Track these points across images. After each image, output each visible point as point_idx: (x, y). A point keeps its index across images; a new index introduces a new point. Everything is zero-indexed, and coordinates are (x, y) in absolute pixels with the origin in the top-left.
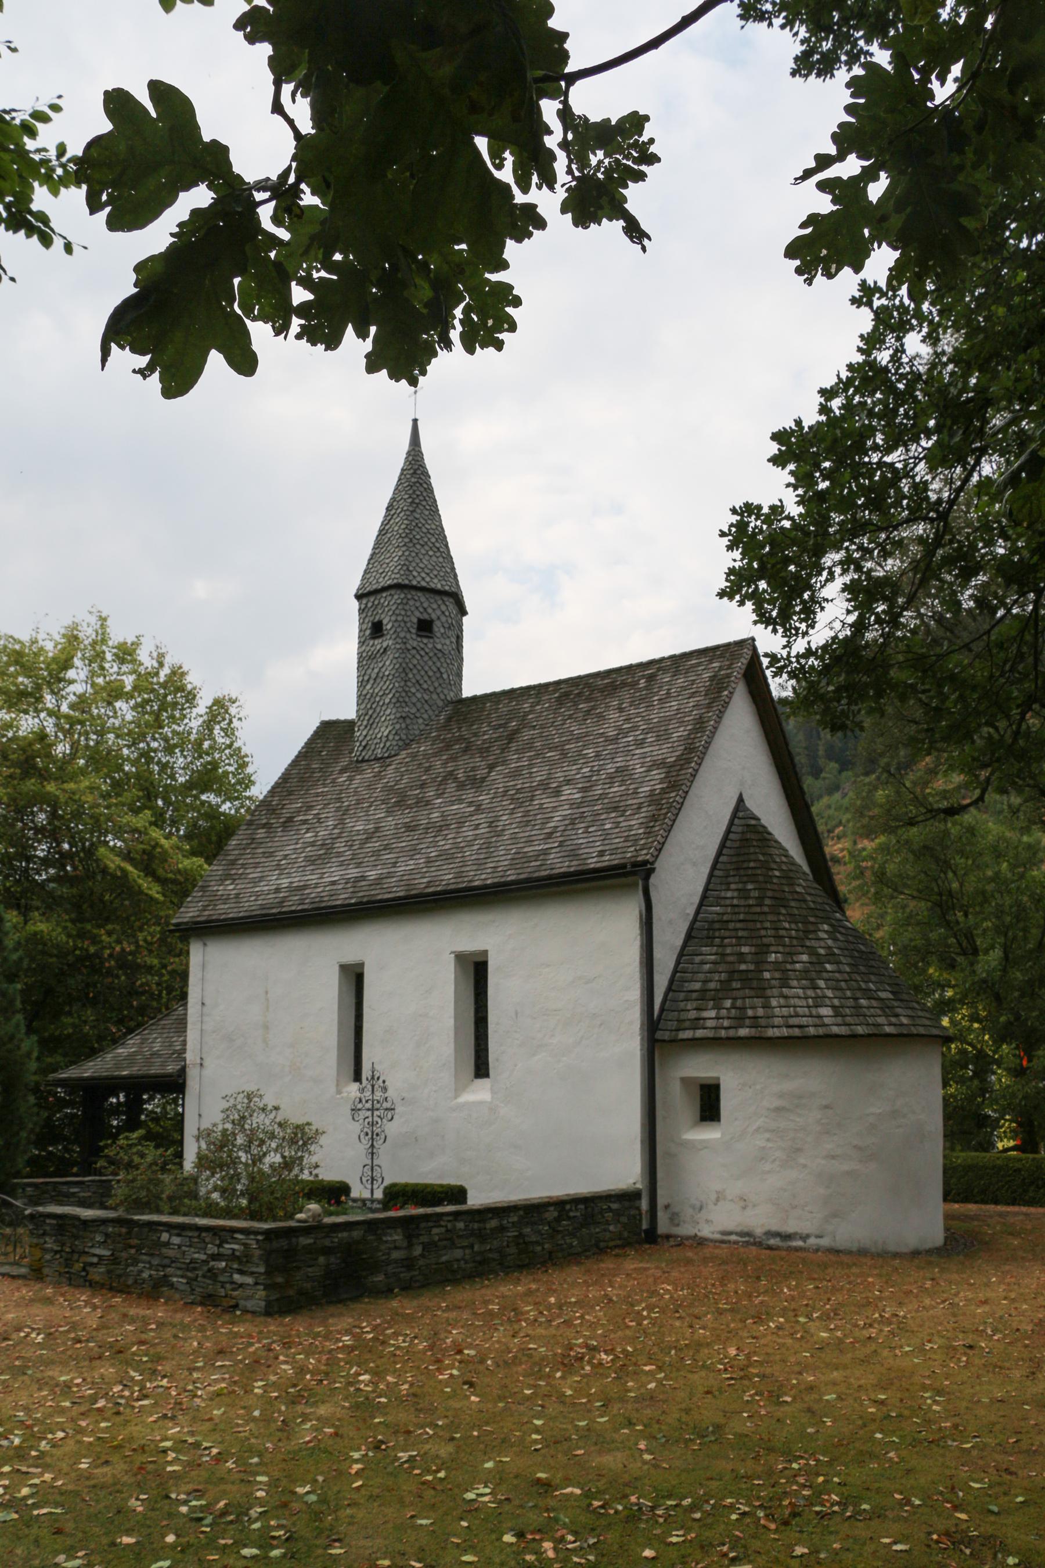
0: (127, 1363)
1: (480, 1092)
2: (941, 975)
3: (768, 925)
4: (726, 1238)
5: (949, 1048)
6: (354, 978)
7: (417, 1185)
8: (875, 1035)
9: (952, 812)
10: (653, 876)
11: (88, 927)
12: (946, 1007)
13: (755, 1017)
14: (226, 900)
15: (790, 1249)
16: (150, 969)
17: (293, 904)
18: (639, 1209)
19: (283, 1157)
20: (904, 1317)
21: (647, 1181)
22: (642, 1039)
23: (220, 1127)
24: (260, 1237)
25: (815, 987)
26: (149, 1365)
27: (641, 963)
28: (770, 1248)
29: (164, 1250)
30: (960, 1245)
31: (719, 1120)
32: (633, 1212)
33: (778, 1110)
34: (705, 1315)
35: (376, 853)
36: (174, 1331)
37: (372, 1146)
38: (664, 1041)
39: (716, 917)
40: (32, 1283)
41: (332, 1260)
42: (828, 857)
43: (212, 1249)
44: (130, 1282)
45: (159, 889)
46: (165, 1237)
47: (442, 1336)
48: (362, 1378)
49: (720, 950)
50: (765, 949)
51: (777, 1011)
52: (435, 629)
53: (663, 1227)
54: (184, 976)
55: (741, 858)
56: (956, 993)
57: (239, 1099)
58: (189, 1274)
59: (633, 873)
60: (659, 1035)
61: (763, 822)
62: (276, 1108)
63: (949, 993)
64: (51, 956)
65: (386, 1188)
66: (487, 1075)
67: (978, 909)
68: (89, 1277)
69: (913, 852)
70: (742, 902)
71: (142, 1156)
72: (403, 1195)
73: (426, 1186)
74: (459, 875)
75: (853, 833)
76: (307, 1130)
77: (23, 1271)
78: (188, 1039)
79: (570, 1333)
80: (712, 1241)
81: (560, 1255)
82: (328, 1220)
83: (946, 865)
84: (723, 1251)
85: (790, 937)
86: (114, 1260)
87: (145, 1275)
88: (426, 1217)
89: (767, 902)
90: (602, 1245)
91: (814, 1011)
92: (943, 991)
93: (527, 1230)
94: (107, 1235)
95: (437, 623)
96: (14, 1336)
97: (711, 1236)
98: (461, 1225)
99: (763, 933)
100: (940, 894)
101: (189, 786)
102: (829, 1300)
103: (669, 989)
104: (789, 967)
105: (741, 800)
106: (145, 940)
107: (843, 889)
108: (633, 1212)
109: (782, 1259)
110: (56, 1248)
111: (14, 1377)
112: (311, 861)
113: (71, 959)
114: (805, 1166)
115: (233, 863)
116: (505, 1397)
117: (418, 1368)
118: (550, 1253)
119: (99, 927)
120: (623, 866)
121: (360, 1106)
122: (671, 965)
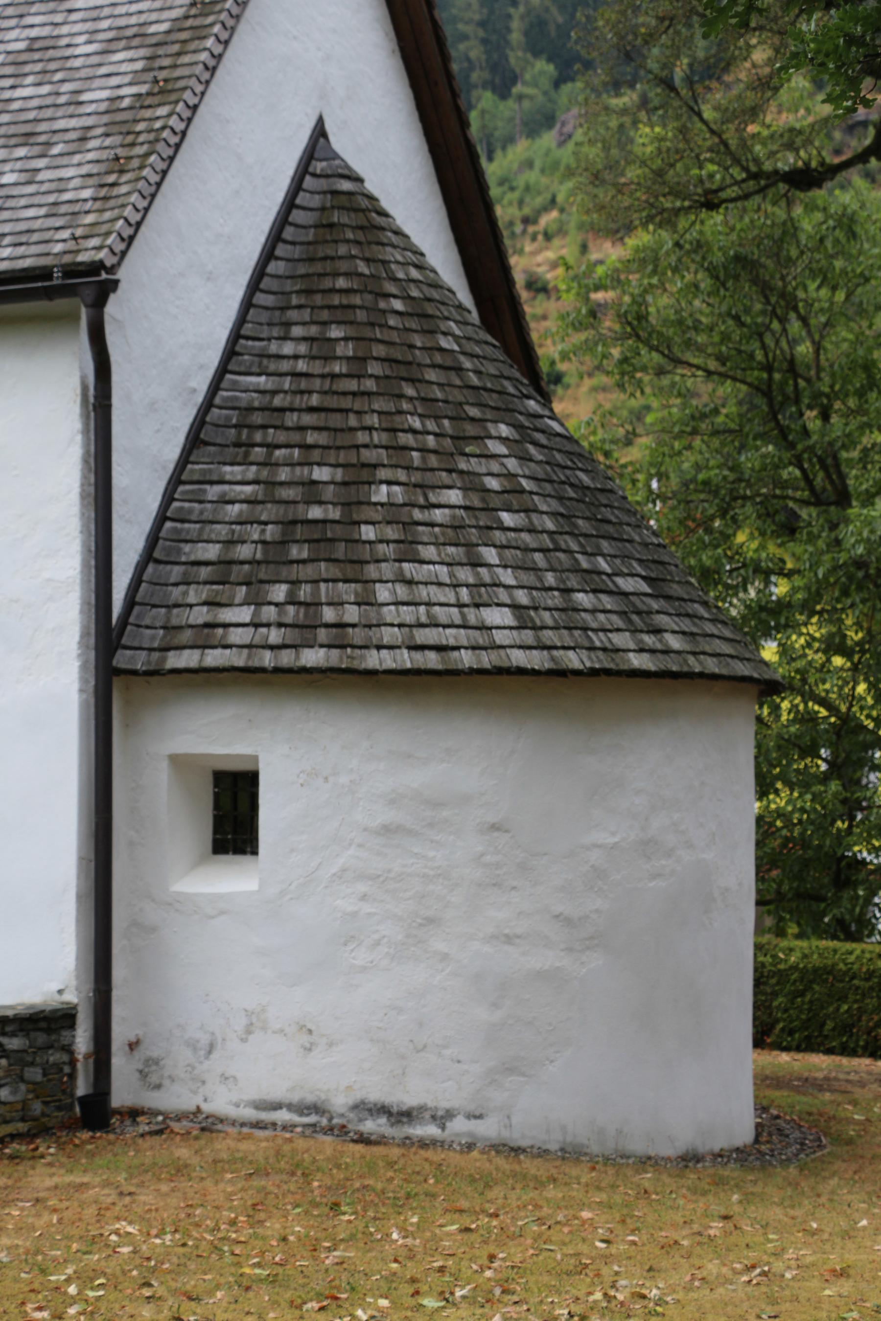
2: (762, 547)
3: (374, 420)
4: (265, 1116)
5: (776, 709)
8: (607, 672)
9: (805, 179)
10: (112, 297)
12: (771, 618)
13: (341, 625)
15: (407, 1142)
18: (68, 1049)
20: (659, 1302)
21: (89, 987)
22: (84, 667)
25: (476, 563)
27: (83, 496)
28: (363, 1140)
30: (786, 1142)
31: (255, 852)
32: (55, 1057)
33: (387, 830)
34: (211, 1293)
38: (134, 673)
39: (257, 400)
42: (519, 278)
49: (265, 473)
50: (365, 475)
51: (389, 613)
53: (122, 1094)
55: (318, 267)
56: (794, 590)
60: (122, 659)
61: (371, 186)
63: (780, 589)
67: (852, 402)
69: (712, 271)
70: (317, 367)
75: (581, 226)
80: (233, 1123)
83: (786, 304)
84: (259, 1146)
85: (423, 450)
89: (374, 368)
91: (472, 616)
92: (767, 583)
99: (362, 437)
100: (769, 368)
102: (492, 1258)
103: (148, 557)
104: (417, 515)
105: (320, 132)
107: (548, 349)
108: (55, 1057)
109: (391, 1164)
114: (445, 957)
120: (44, 273)
122: (153, 504)
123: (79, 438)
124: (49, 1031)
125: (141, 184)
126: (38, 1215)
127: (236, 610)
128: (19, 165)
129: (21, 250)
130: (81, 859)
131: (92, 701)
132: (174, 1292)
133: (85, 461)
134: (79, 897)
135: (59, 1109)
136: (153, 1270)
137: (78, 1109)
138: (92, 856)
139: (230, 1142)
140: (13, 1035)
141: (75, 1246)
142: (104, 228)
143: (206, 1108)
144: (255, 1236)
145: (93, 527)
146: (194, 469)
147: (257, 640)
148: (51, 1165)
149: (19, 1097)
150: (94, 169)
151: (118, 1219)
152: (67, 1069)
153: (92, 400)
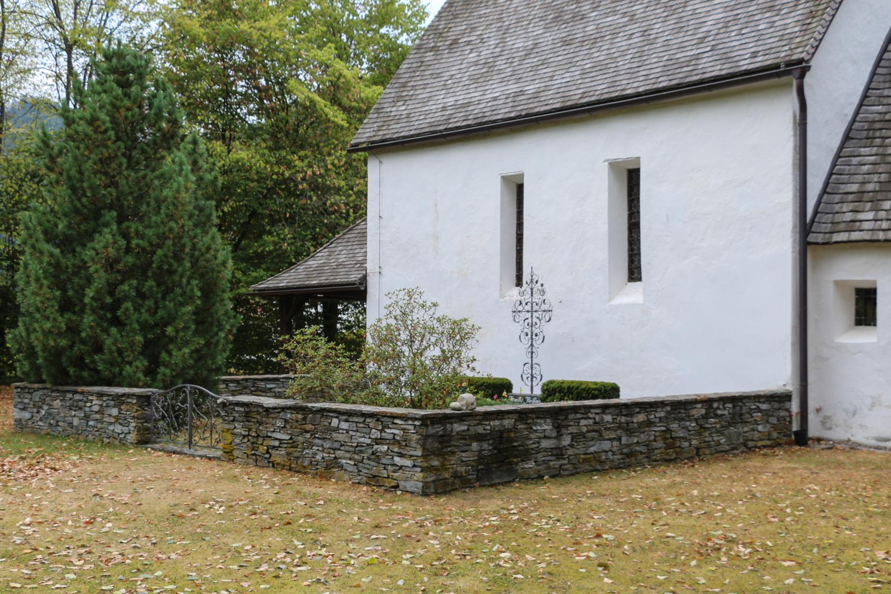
0: (293, 533)
1: (634, 294)
7: (572, 382)
10: (808, 75)
11: (284, 153)
14: (398, 121)
16: (338, 190)
17: (458, 121)
18: (788, 410)
19: (443, 351)
22: (794, 242)
23: (384, 324)
24: (417, 423)
26: (312, 536)
27: (794, 165)
29: (334, 435)
31: (875, 325)
32: (782, 413)
34: (853, 517)
35: (534, 68)
36: (339, 507)
37: (532, 345)
38: (817, 244)
39: (877, 117)
40: (225, 464)
41: (485, 446)
43: (375, 434)
44: (306, 464)
45: (344, 117)
46: (335, 422)
47: (584, 521)
48: (502, 555)
49: (881, 150)
53: (814, 430)
54: (363, 195)
57: (401, 296)
58: (356, 457)
59: (787, 73)
60: (811, 238)
62: (435, 305)
64: (252, 181)
65: (544, 385)
66: (640, 279)
68: (272, 459)
71: (316, 348)
72: (560, 392)
73: (581, 383)
74: (613, 84)
76: (464, 325)
77: (219, 453)
78: (368, 250)
79: (709, 524)
80: (866, 446)
81: (707, 451)
82: (478, 409)
86: (293, 444)
87: (319, 457)
88: (575, 409)
90: (750, 444)
93: (674, 426)
94: (286, 421)
96: (200, 508)
97: (865, 442)
98: (608, 418)
101: (370, 20)
103: (824, 191)
106: (333, 164)
110: (244, 433)
111: (193, 542)
112: (474, 79)
113: (270, 183)
115: (404, 85)
116: (638, 581)
117: (557, 548)
118: (698, 449)
119: (293, 153)
120: (777, 66)
121: (520, 308)
123: (792, 139)
124: (779, 402)
125: (822, 22)
126: (774, 479)
127: (866, 214)
128: (767, 20)
129: (767, 57)
130: (793, 327)
131: (798, 256)
132: (835, 515)
133: (795, 149)
134: (793, 344)
135: (785, 436)
136: (826, 505)
137: (793, 437)
138: (798, 326)
139: (864, 455)
140: (764, 403)
141: (790, 493)
142: (804, 43)
143: (853, 439)
144: (875, 495)
145: (798, 178)
146: (846, 151)
147: (876, 227)
148: (781, 459)
149: (766, 430)
150: (801, 18)
151: (810, 483)
152: (788, 419)
153: (798, 121)
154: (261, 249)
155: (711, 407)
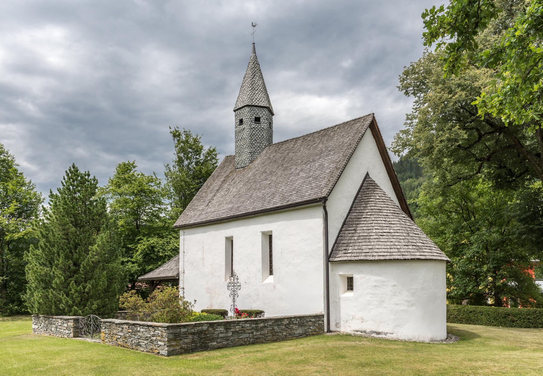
6: (230, 241)
32: (320, 322)
33: (375, 286)
43: (152, 333)
46: (139, 329)
52: (261, 120)
61: (376, 182)
93: (276, 328)
95: (262, 118)
105: (367, 174)
114: (386, 307)
146: (344, 229)
154: (442, 228)
155: (291, 320)
